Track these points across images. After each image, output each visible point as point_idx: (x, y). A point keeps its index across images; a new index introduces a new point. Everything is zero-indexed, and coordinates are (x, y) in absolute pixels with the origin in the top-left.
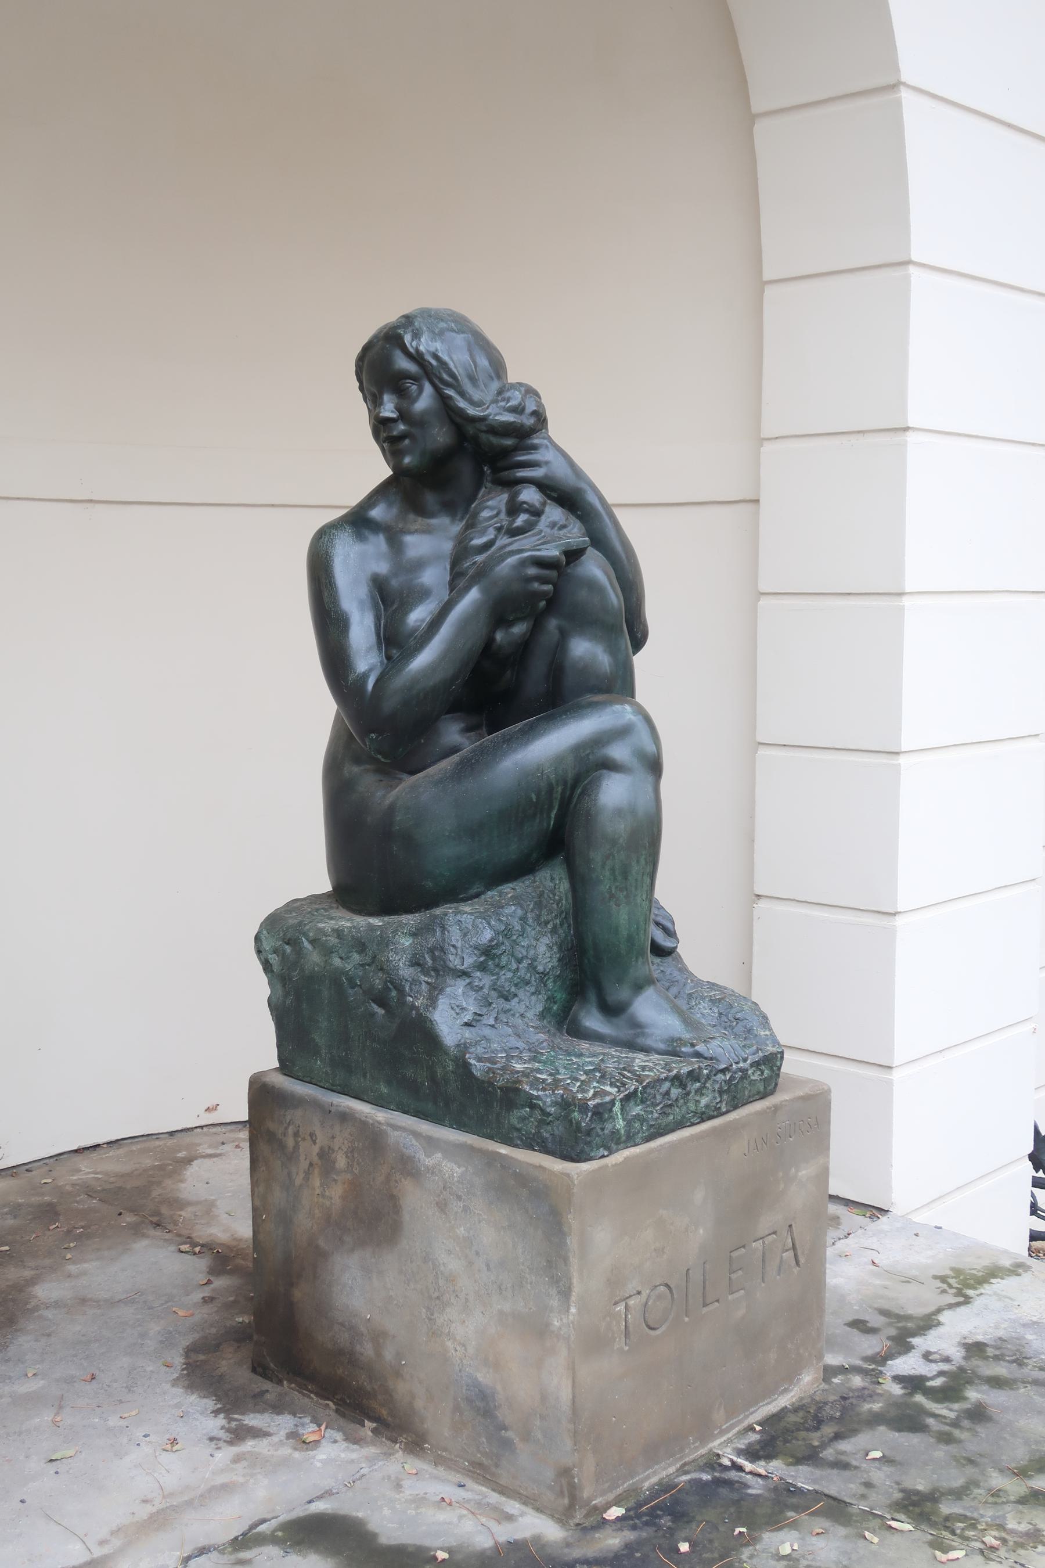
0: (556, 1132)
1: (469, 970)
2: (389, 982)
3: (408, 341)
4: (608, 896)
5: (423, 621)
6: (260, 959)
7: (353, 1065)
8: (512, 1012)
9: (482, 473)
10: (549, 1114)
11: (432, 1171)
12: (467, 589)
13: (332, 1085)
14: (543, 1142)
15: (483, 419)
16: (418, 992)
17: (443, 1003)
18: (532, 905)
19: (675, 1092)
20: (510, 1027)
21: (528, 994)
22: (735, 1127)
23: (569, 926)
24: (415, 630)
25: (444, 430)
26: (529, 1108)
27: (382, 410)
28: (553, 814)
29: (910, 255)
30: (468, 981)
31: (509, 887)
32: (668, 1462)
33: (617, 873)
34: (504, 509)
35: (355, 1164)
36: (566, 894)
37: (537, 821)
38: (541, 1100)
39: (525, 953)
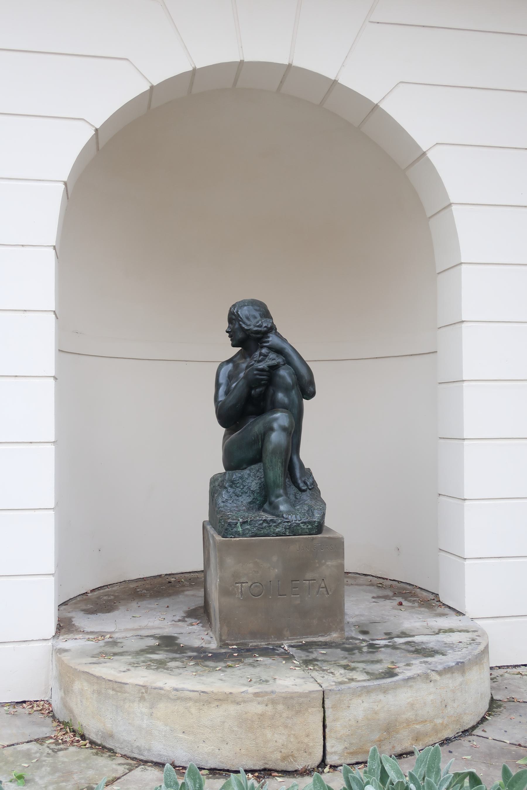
15: (249, 330)
32: (261, 640)
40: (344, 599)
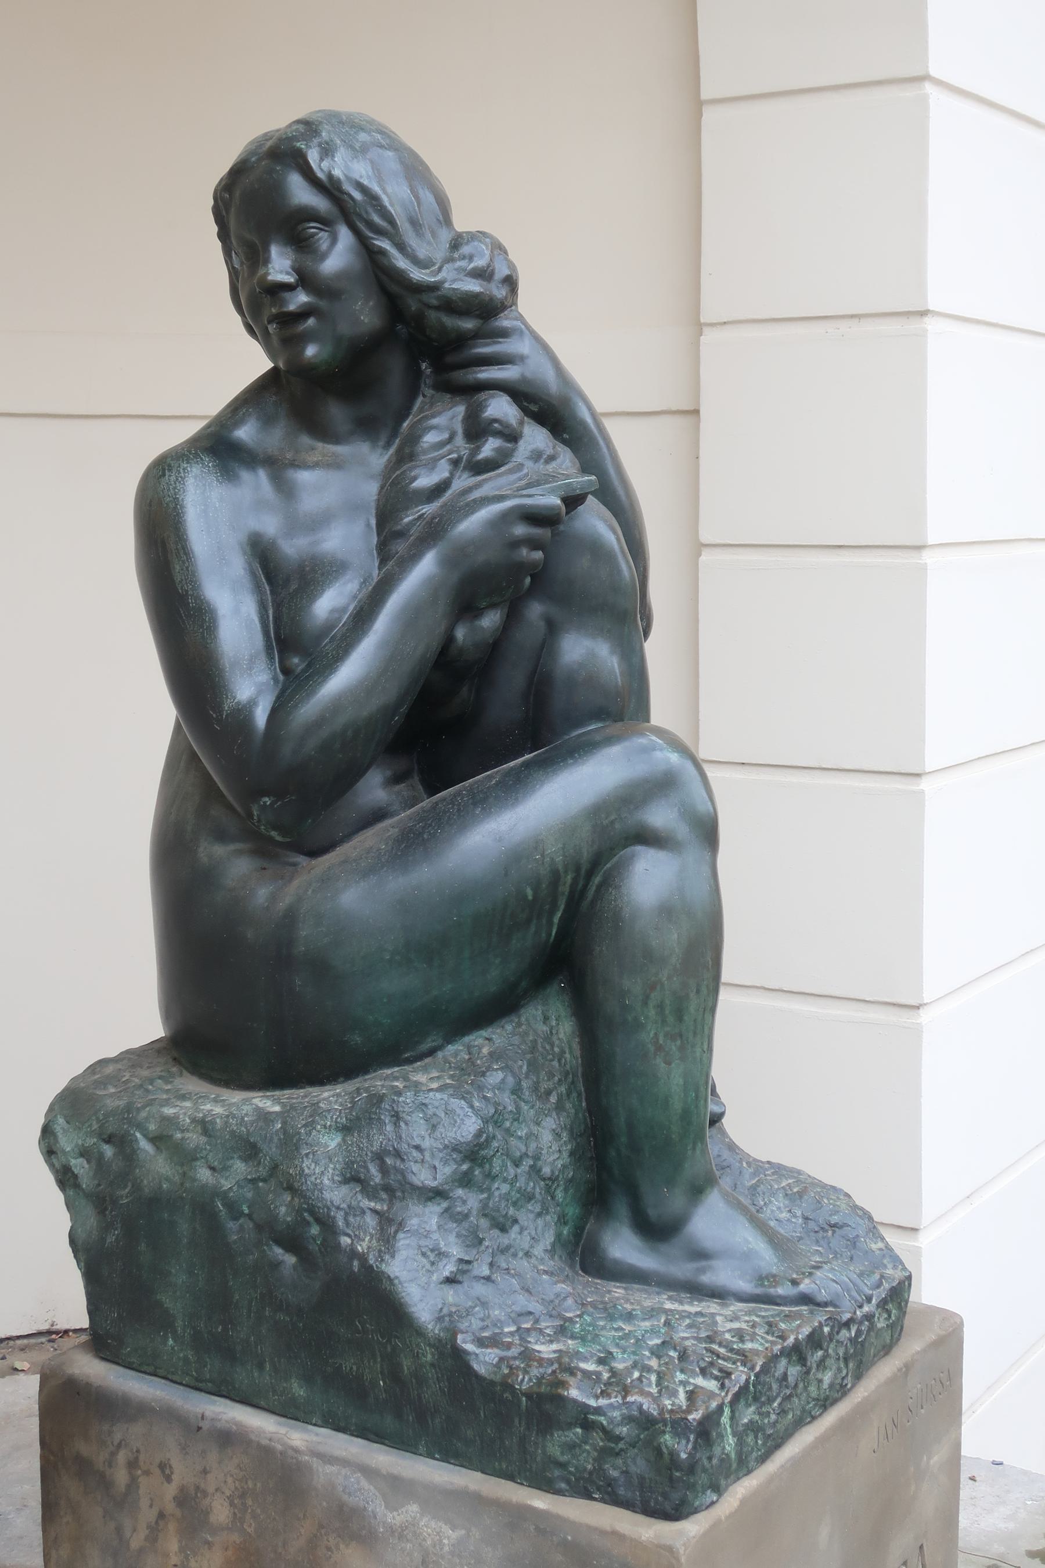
0: (633, 1469)
1: (446, 1187)
2: (306, 1210)
3: (314, 161)
4: (652, 1049)
5: (344, 610)
6: (51, 1166)
7: (239, 1348)
8: (512, 1250)
9: (418, 374)
10: (619, 1439)
11: (400, 1533)
12: (413, 557)
13: (197, 1380)
14: (609, 1485)
16: (359, 1227)
17: (404, 1243)
18: (525, 1067)
19: (794, 1371)
20: (513, 1276)
21: (531, 1216)
22: (862, 1411)
23: (579, 1095)
24: (328, 627)
25: (371, 303)
26: (582, 1428)
27: (271, 271)
28: (556, 920)
29: (927, 67)
30: (445, 1205)
31: (481, 1037)
33: (667, 1012)
34: (460, 429)
35: (248, 1516)
36: (569, 1042)
37: (533, 929)
38: (604, 1414)
39: (523, 1149)
40: (386, 1276)
